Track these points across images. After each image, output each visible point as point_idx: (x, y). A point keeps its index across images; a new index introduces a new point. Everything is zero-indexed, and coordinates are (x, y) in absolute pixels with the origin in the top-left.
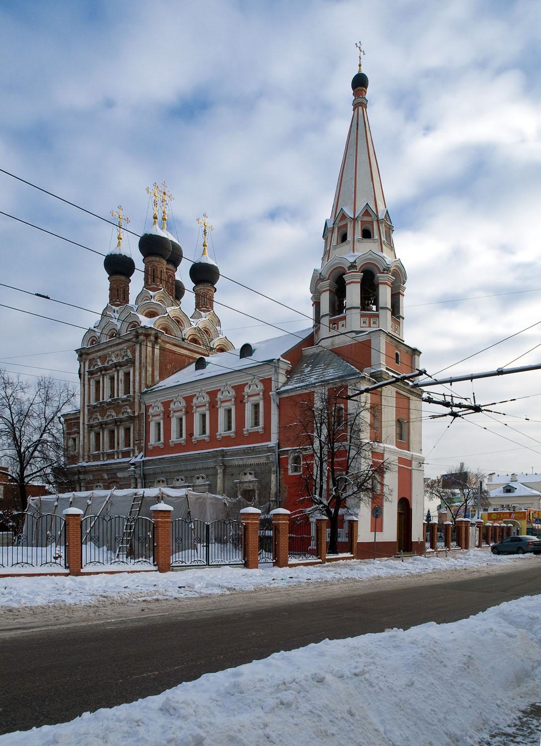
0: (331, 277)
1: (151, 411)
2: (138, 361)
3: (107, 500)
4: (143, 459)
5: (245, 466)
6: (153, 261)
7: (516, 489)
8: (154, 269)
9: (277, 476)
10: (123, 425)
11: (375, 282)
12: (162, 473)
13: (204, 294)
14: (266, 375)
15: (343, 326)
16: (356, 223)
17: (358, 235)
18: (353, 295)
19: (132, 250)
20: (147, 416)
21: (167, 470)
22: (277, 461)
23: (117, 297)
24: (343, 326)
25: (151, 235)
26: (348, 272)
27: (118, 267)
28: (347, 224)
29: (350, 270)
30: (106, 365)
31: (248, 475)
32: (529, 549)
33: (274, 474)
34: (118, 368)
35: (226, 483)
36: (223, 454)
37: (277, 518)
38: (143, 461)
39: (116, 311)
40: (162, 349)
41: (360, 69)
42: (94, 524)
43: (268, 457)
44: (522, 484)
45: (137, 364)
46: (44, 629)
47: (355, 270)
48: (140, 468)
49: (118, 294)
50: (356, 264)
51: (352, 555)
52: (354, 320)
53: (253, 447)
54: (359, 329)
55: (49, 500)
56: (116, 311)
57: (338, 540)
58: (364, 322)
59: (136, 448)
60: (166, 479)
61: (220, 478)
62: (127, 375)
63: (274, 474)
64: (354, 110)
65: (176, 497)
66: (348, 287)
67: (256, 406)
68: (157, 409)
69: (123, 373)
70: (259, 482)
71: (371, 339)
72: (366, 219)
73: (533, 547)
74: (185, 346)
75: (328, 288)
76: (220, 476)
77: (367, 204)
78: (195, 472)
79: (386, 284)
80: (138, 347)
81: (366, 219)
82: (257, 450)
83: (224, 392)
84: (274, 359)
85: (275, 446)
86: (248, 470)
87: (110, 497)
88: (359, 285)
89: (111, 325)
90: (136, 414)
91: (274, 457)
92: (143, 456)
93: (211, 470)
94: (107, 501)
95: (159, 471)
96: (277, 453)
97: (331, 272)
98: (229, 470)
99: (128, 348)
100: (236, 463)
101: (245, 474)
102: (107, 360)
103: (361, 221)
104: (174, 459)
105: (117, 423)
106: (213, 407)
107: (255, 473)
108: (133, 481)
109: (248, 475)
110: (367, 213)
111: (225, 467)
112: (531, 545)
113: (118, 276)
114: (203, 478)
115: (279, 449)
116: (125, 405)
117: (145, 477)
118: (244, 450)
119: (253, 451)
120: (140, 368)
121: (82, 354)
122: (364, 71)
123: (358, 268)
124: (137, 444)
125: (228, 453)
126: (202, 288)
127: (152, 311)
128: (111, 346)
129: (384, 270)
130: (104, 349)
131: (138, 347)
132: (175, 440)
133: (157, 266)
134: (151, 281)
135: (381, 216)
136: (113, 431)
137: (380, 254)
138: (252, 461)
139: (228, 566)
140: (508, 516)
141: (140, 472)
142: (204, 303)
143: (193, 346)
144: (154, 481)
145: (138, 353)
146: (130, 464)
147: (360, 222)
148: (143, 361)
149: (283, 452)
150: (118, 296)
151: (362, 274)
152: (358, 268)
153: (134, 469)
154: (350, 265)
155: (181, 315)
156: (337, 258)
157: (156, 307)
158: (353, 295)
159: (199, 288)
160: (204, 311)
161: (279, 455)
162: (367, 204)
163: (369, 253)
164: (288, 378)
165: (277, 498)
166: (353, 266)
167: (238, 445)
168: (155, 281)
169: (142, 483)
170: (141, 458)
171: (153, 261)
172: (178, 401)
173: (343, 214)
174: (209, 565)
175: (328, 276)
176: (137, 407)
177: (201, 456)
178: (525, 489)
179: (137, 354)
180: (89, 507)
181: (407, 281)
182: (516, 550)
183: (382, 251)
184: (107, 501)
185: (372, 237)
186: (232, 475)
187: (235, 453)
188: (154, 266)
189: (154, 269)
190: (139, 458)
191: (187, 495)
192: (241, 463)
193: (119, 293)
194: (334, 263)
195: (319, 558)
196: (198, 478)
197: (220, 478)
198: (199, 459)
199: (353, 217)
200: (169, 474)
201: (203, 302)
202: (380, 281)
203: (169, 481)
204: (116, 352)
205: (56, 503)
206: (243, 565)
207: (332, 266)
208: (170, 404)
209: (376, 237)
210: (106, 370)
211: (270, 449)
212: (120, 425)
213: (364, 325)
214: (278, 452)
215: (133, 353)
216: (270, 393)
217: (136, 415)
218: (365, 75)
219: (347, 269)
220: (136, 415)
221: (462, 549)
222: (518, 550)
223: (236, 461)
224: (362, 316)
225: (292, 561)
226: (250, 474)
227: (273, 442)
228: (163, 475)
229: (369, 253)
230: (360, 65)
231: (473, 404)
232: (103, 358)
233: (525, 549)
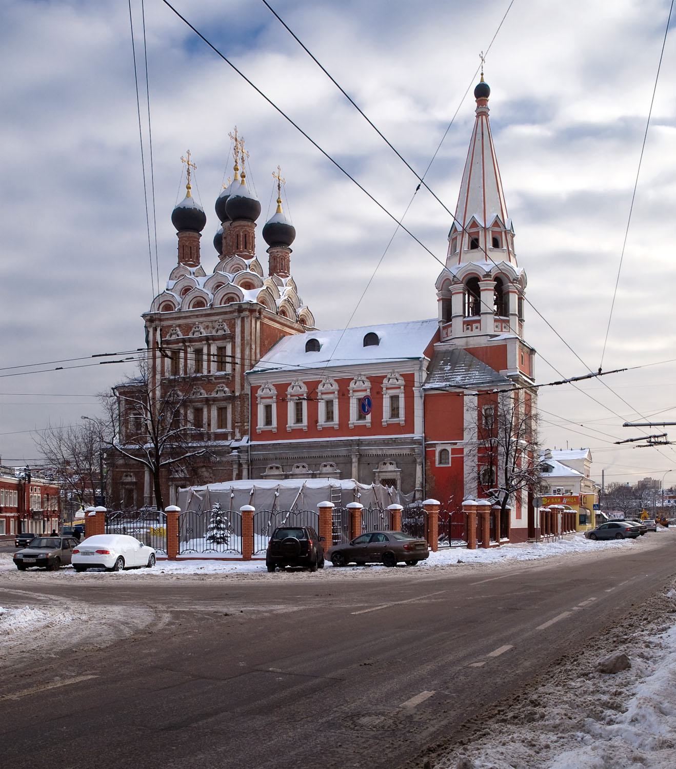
0: (464, 282)
1: (259, 393)
2: (240, 337)
3: (300, 492)
4: (250, 443)
5: (385, 456)
6: (245, 226)
7: (554, 467)
8: (246, 235)
9: (422, 467)
10: (215, 404)
11: (505, 291)
12: (276, 459)
13: (281, 257)
14: (407, 370)
15: (477, 328)
16: (487, 233)
17: (490, 245)
18: (488, 299)
19: (206, 203)
20: (254, 398)
21: (284, 456)
22: (424, 453)
23: (190, 256)
24: (477, 328)
25: (244, 197)
26: (482, 279)
27: (188, 221)
28: (479, 232)
29: (485, 278)
30: (191, 336)
31: (388, 465)
32: (627, 535)
33: (420, 465)
34: (210, 342)
35: (361, 472)
36: (359, 443)
37: (484, 508)
38: (251, 445)
39: (192, 273)
40: (262, 324)
41: (482, 78)
42: (289, 515)
43: (413, 449)
44: (558, 461)
45: (238, 340)
46: (280, 608)
47: (490, 279)
48: (248, 452)
49: (188, 253)
50: (491, 274)
51: (508, 540)
52: (488, 323)
53: (395, 438)
54: (493, 333)
55: (221, 491)
56: (192, 273)
57: (497, 528)
58: (497, 327)
59: (237, 430)
60: (283, 466)
61: (355, 467)
62: (222, 349)
63: (420, 465)
64: (477, 117)
65: (368, 489)
66: (482, 293)
67: (394, 399)
68: (267, 392)
69: (216, 348)
70: (402, 472)
71: (506, 345)
72: (496, 229)
73: (631, 532)
74: (278, 319)
75: (462, 291)
76: (355, 465)
77: (497, 216)
78: (322, 460)
79: (515, 292)
80: (239, 322)
81: (496, 229)
82: (399, 441)
83: (357, 382)
84: (421, 358)
85: (422, 439)
86: (387, 460)
87: (302, 489)
88: (483, 289)
89: (197, 293)
90: (237, 394)
91: (418, 449)
92: (248, 440)
93: (341, 459)
94: (300, 493)
95: (271, 456)
96: (424, 445)
97: (467, 274)
98: (364, 459)
99: (224, 321)
100: (374, 452)
101: (385, 464)
102: (192, 331)
103: (492, 231)
104: (294, 445)
105: (207, 402)
106: (343, 395)
107: (396, 463)
108: (235, 466)
109: (388, 465)
110: (496, 224)
111: (361, 457)
112: (630, 531)
113: (191, 233)
114: (331, 466)
115: (425, 442)
116: (220, 383)
117: (251, 463)
118: (384, 440)
119: (394, 441)
120: (243, 345)
121: (150, 319)
122: (486, 81)
123: (492, 277)
124: (237, 426)
125: (363, 442)
126: (278, 250)
127: (247, 282)
128: (197, 316)
129: (514, 280)
130: (185, 318)
131: (239, 322)
132: (292, 425)
133: (249, 231)
134: (243, 247)
135: (508, 227)
136: (201, 410)
137: (508, 263)
138: (393, 452)
139: (460, 548)
140: (559, 500)
141: (246, 457)
142: (279, 267)
143: (284, 319)
144: (266, 468)
145: (240, 329)
146: (231, 448)
147: (491, 231)
148: (247, 337)
149: (429, 445)
150: (191, 254)
151: (496, 283)
152: (492, 277)
153: (237, 454)
154: (486, 273)
155: (271, 285)
156: (472, 265)
157: (251, 277)
158: (488, 299)
159: (276, 250)
160: (282, 276)
161: (425, 448)
162: (497, 216)
163: (501, 265)
164: (428, 374)
165: (423, 488)
166: (488, 275)
167: (374, 435)
168: (247, 248)
169: (248, 469)
170: (248, 442)
171: (245, 226)
172: (299, 386)
173: (474, 222)
174: (450, 546)
175: (462, 278)
176: (238, 387)
177: (329, 444)
178: (564, 468)
179: (238, 330)
180: (277, 498)
181: (527, 286)
182: (614, 535)
183: (510, 261)
184: (300, 493)
185: (500, 246)
186: (369, 464)
187: (370, 443)
188: (245, 231)
189: (246, 235)
190: (244, 442)
191: (373, 488)
192: (380, 453)
193: (193, 251)
194: (468, 268)
195: (496, 542)
196: (325, 466)
197: (355, 467)
198: (327, 447)
199: (484, 226)
200: (286, 461)
201: (281, 266)
202: (510, 290)
203: (284, 468)
204: (204, 323)
205: (232, 495)
206: (466, 547)
207: (466, 271)
208: (288, 387)
209: (505, 248)
210: (190, 342)
211: (414, 442)
212: (213, 404)
213: (496, 329)
214: (425, 444)
215: (232, 327)
216: (414, 388)
217: (236, 395)
218: (488, 86)
219: (481, 277)
220: (236, 395)
221: (555, 536)
222: (616, 535)
223: (374, 450)
224: (496, 321)
225: (491, 544)
226: (391, 464)
227: (418, 433)
228: (278, 461)
229: (501, 265)
230: (482, 74)
231: (665, 441)
232: (187, 329)
233: (624, 535)
